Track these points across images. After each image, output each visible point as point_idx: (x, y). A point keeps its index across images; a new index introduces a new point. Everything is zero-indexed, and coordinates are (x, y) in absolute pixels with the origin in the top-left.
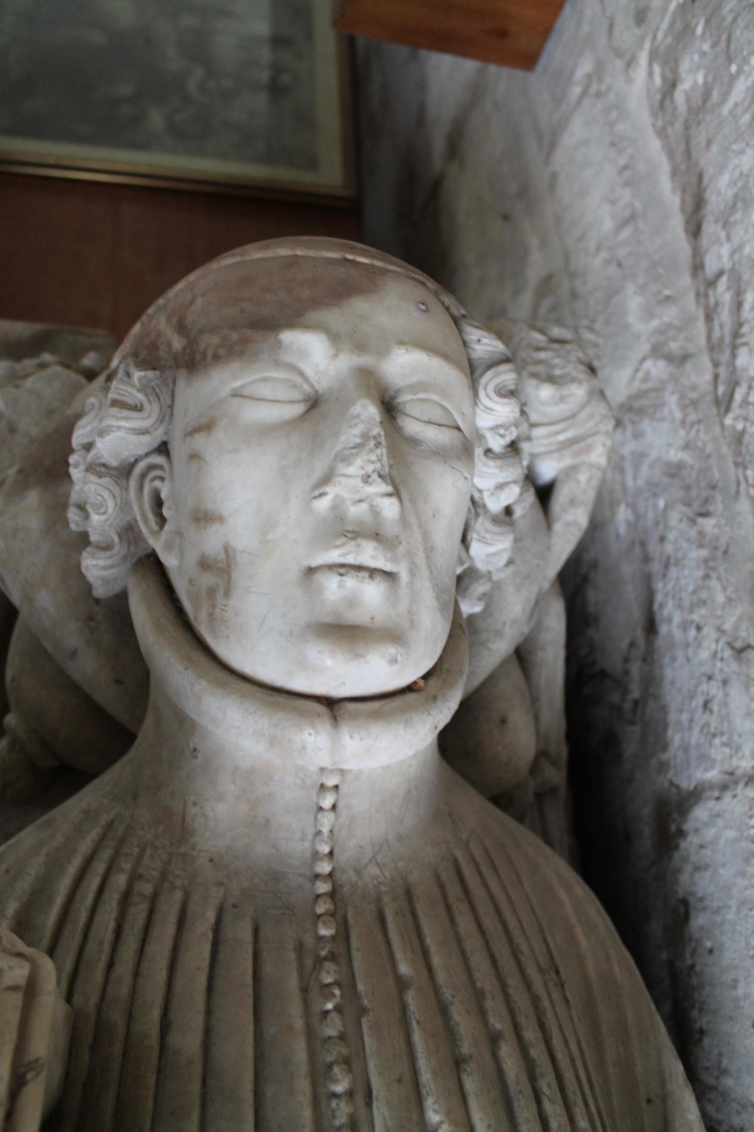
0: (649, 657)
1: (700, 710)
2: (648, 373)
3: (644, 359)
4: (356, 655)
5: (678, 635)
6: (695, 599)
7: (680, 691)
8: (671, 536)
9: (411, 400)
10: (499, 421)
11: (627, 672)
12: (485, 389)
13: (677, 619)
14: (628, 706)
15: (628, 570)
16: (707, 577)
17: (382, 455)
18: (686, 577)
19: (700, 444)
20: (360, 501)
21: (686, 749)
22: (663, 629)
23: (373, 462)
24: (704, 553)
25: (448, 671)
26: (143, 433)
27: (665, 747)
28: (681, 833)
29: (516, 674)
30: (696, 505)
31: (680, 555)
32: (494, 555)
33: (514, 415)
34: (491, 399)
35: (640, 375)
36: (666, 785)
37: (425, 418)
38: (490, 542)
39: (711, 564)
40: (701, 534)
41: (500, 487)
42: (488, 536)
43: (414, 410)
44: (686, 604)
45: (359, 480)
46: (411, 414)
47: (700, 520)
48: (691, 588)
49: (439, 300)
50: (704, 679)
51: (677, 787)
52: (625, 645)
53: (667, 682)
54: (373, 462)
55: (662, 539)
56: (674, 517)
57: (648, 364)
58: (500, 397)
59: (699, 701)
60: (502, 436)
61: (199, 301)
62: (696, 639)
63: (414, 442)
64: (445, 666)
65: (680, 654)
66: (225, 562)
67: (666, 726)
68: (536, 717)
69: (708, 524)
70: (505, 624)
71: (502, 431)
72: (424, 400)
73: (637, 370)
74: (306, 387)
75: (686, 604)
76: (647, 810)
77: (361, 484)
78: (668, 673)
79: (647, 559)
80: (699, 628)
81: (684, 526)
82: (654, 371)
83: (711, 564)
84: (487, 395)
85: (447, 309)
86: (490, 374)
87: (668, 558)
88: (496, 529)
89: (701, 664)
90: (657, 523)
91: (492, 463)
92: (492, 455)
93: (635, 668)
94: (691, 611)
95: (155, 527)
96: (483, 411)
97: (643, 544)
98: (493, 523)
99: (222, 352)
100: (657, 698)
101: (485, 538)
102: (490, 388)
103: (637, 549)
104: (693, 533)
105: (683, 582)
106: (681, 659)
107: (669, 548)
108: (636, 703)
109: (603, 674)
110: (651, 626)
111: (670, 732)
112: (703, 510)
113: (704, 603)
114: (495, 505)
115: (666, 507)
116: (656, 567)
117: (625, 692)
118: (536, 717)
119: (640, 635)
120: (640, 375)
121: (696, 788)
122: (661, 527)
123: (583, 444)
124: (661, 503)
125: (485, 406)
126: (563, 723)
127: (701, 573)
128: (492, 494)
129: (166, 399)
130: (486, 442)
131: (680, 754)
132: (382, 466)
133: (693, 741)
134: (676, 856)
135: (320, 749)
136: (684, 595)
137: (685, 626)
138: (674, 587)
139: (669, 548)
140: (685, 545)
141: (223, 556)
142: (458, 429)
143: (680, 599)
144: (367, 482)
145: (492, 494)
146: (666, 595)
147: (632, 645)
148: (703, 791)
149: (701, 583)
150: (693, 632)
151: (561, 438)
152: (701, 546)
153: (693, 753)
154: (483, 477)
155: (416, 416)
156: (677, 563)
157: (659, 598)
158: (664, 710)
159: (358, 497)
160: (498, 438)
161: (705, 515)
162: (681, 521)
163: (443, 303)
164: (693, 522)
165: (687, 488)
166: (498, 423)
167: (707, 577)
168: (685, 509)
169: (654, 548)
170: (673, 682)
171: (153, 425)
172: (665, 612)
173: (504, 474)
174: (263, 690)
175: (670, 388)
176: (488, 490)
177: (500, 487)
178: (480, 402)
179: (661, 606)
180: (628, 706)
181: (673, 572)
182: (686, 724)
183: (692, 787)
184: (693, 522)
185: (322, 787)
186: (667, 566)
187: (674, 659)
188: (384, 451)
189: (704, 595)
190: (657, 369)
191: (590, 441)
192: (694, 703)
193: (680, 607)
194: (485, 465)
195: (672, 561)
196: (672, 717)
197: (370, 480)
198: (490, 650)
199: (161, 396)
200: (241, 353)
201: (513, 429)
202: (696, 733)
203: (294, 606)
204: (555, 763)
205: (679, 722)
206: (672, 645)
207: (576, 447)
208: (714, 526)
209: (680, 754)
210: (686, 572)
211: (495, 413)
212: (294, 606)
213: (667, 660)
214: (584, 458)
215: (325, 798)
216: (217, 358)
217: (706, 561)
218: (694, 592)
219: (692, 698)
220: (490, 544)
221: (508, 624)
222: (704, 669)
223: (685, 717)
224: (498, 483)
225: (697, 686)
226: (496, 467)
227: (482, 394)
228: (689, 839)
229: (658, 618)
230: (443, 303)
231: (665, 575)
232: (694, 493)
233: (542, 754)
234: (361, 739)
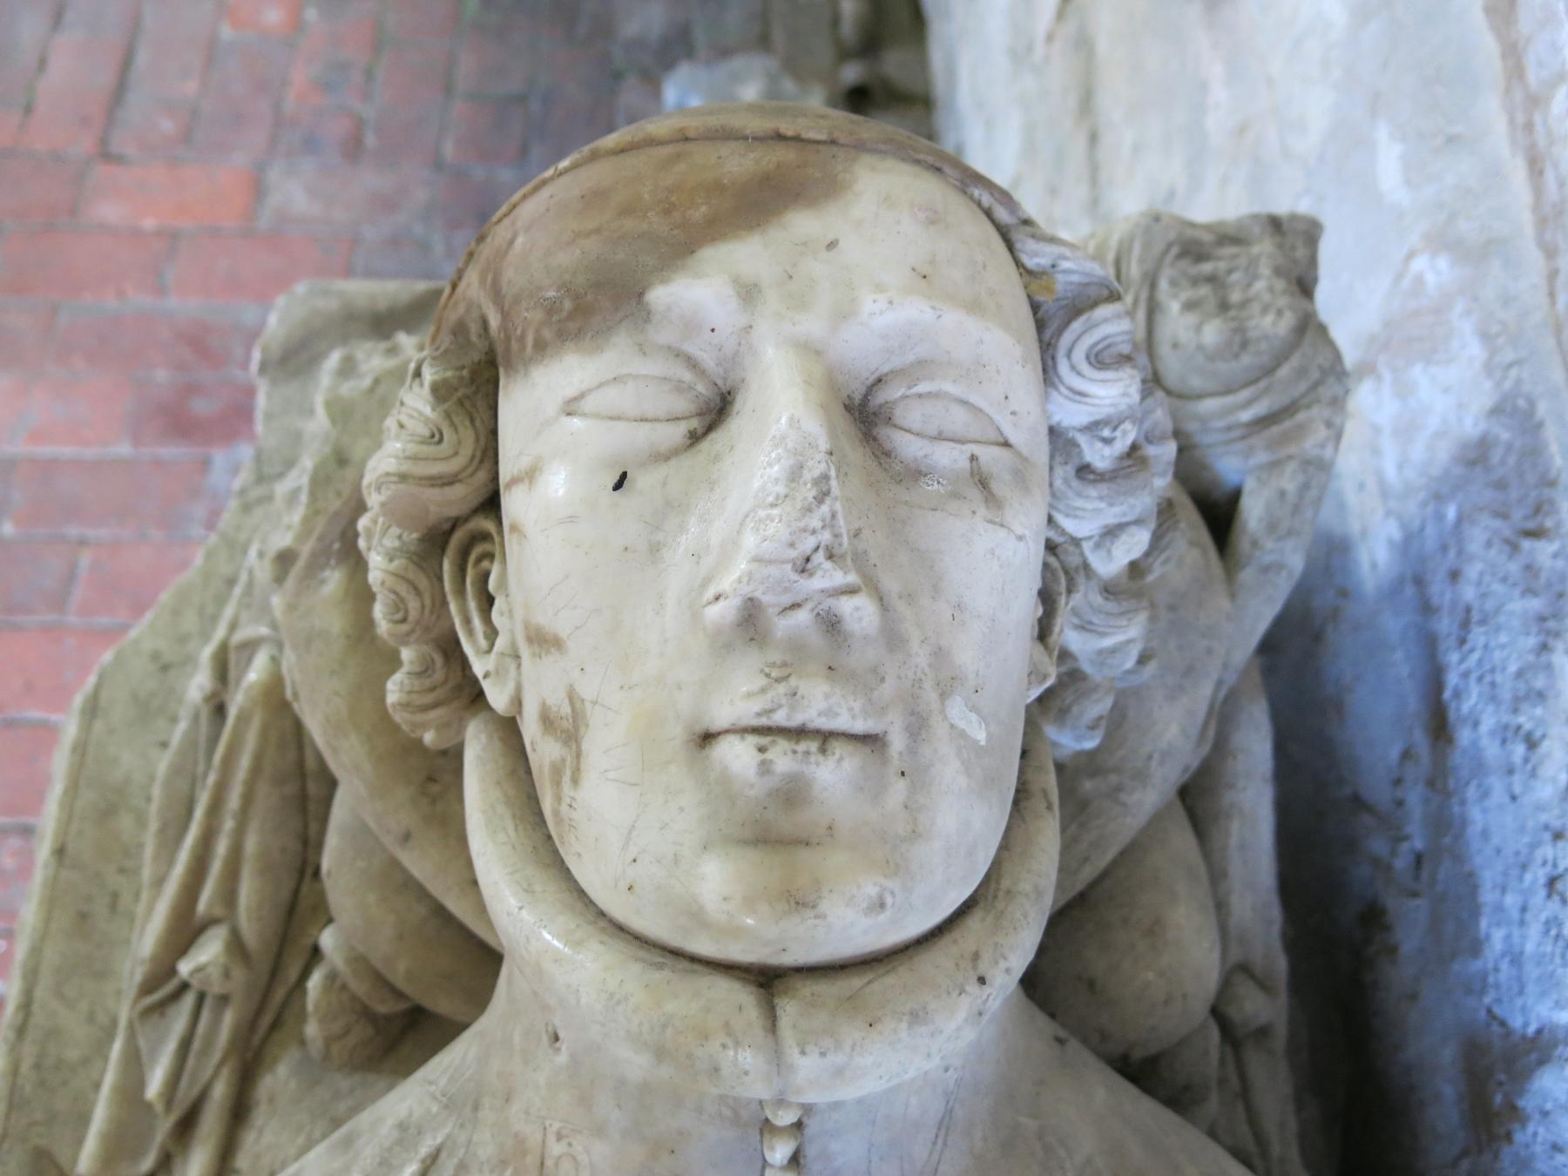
0: (1439, 782)
1: (1543, 893)
2: (1419, 280)
3: (1411, 255)
4: (798, 903)
5: (1491, 750)
6: (1522, 687)
7: (1498, 851)
8: (1472, 571)
9: (905, 397)
10: (1099, 414)
11: (1400, 803)
12: (1069, 354)
13: (1488, 722)
14: (1401, 863)
15: (1394, 624)
16: (1544, 648)
17: (833, 516)
18: (1503, 646)
19: (1521, 403)
20: (795, 606)
21: (1516, 959)
22: (1464, 736)
23: (814, 532)
24: (1536, 604)
25: (1009, 892)
26: (450, 484)
27: (1476, 947)
28: (1514, 1112)
29: (1182, 839)
30: (1518, 515)
31: (1490, 605)
32: (1113, 651)
33: (1127, 400)
34: (1079, 373)
35: (1406, 283)
36: (1482, 1014)
37: (932, 430)
38: (1101, 629)
39: (1551, 624)
40: (1530, 569)
41: (1111, 532)
42: (1095, 620)
43: (912, 415)
44: (1506, 694)
45: (789, 567)
46: (906, 424)
47: (1526, 544)
48: (1513, 668)
49: (971, 198)
50: (1547, 836)
51: (1503, 1023)
52: (1395, 753)
53: (1474, 830)
54: (814, 532)
55: (1455, 575)
56: (1476, 538)
57: (1420, 264)
58: (1100, 369)
59: (1540, 874)
60: (1108, 441)
61: (520, 240)
62: (1526, 760)
63: (916, 473)
64: (1005, 883)
65: (1497, 785)
66: (571, 721)
67: (1475, 912)
68: (1221, 907)
69: (1543, 552)
70: (1150, 757)
71: (1106, 433)
72: (929, 395)
73: (1399, 277)
74: (701, 388)
75: (1506, 694)
76: (1448, 1055)
77: (794, 577)
78: (1476, 815)
79: (1427, 609)
80: (1532, 743)
81: (1496, 554)
82: (1430, 279)
83: (1551, 624)
84: (1073, 368)
85: (988, 213)
86: (1077, 325)
87: (1468, 610)
88: (1111, 606)
89: (1540, 808)
90: (1444, 548)
91: (1093, 492)
92: (1092, 477)
93: (1415, 797)
94: (1515, 711)
95: (483, 643)
96: (1066, 397)
97: (1419, 582)
98: (1106, 595)
99: (547, 334)
100: (1459, 858)
101: (1091, 623)
102: (1079, 355)
103: (1410, 591)
104: (1514, 567)
105: (1497, 655)
106: (1498, 795)
107: (1469, 593)
108: (1419, 859)
109: (1358, 803)
110: (1439, 725)
111: (1484, 923)
112: (1531, 525)
113: (1541, 696)
114: (1111, 563)
115: (1460, 520)
116: (1445, 625)
117: (1399, 838)
118: (1221, 907)
119: (1420, 739)
120: (1406, 283)
121: (1539, 1032)
122: (1452, 553)
123: (1287, 424)
124: (1451, 512)
125: (1071, 389)
126: (1276, 913)
127: (1532, 641)
128: (1098, 546)
129: (482, 414)
130: (1080, 453)
131: (1504, 966)
132: (836, 536)
133: (1530, 947)
134: (1506, 1153)
135: (746, 1073)
136: (1499, 678)
137: (1506, 734)
138: (1480, 662)
139: (1469, 593)
140: (1498, 587)
141: (566, 710)
142: (1006, 444)
143: (1493, 684)
144: (803, 571)
145: (1098, 546)
146: (1466, 675)
147: (1406, 755)
148: (1554, 1044)
149: (1531, 658)
150: (1519, 750)
151: (1246, 416)
152: (1529, 591)
153: (1531, 971)
154: (1076, 517)
155: (916, 426)
156: (1483, 622)
157: (1452, 679)
158: (1471, 884)
159: (787, 600)
160: (1099, 445)
161: (1536, 534)
162: (1489, 544)
163: (979, 204)
164: (1514, 548)
165: (1501, 485)
166: (1097, 417)
167: (1544, 648)
168: (1497, 523)
169: (1438, 589)
170: (1485, 834)
171: (464, 469)
172: (1466, 707)
173: (1116, 510)
174: (642, 954)
175: (1459, 307)
176: (1090, 538)
177: (1111, 532)
178: (1059, 377)
179: (1457, 694)
180: (1401, 863)
181: (1478, 636)
182: (1515, 914)
183: (1531, 1030)
184: (1514, 548)
185: (767, 1127)
186: (1465, 625)
187: (1485, 794)
188: (838, 506)
189: (1539, 683)
190: (1435, 271)
191: (1301, 417)
192: (1528, 877)
193: (1494, 699)
194: (1079, 495)
195: (1475, 616)
196: (1487, 896)
197: (809, 566)
198: (1124, 805)
199: (475, 415)
200: (578, 335)
201: (1127, 426)
202: (1534, 930)
203: (681, 809)
204: (1264, 985)
205: (1499, 908)
206: (1480, 768)
207: (1275, 430)
208: (1555, 556)
209: (1504, 966)
210: (1503, 638)
211: (1087, 400)
212: (681, 809)
213: (1471, 792)
214: (1292, 449)
215: (772, 1149)
216: (541, 347)
217: (1542, 619)
218: (1520, 674)
219: (1524, 867)
220: (1103, 635)
221: (1156, 756)
222: (1544, 817)
223: (1511, 900)
224: (1106, 526)
225: (1534, 846)
226: (1101, 498)
227: (1063, 367)
228: (1531, 1128)
229: (1452, 715)
230: (979, 204)
231: (1462, 641)
232: (1514, 494)
233: (1238, 971)
234: (823, 1054)
